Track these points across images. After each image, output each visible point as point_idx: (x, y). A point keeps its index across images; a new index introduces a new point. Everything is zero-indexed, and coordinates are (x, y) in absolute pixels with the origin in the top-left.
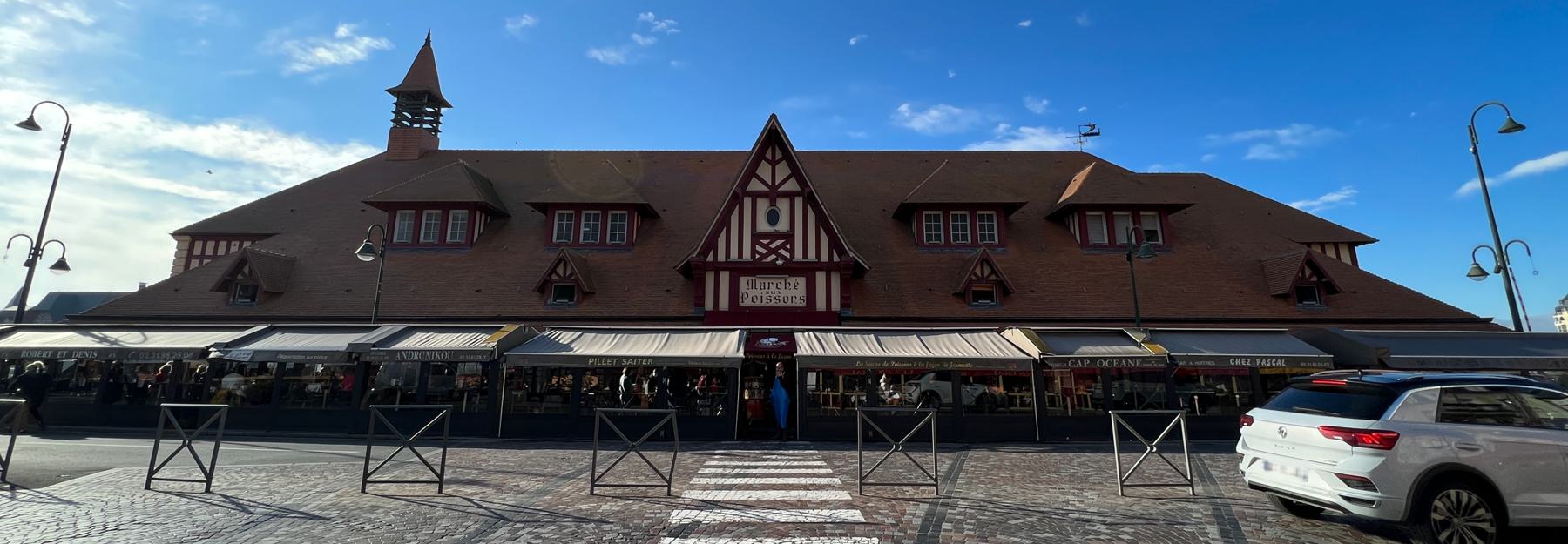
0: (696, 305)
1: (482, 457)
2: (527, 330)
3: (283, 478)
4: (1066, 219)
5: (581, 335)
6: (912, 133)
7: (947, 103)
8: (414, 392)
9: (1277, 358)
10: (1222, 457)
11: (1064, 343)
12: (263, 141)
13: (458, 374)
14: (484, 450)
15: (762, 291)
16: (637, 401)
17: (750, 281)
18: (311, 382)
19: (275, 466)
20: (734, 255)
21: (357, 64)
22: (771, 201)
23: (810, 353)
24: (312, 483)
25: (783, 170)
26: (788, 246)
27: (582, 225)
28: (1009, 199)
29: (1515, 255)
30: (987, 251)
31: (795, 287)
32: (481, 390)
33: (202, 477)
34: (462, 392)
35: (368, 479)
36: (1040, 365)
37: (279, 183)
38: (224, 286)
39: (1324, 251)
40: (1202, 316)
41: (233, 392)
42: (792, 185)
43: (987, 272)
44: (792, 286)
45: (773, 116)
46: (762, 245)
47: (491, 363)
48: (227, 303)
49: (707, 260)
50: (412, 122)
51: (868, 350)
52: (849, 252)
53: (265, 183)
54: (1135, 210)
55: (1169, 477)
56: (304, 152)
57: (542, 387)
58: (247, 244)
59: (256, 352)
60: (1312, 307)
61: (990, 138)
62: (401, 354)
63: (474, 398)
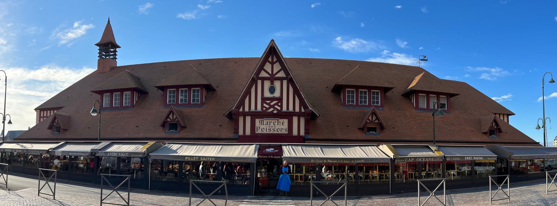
0: (235, 133)
1: (144, 197)
2: (158, 144)
3: (75, 198)
4: (410, 96)
5: (181, 146)
6: (342, 51)
7: (360, 38)
8: (115, 169)
9: (480, 157)
10: (458, 195)
11: (402, 151)
12: (55, 72)
13: (131, 163)
14: (144, 195)
15: (267, 126)
16: (208, 177)
17: (261, 121)
18: (80, 164)
19: (72, 193)
20: (253, 108)
21: (83, 36)
22: (271, 82)
23: (289, 156)
24: (84, 201)
25: (277, 67)
26: (280, 104)
27: (180, 95)
28: (387, 85)
29: (547, 121)
30: (375, 109)
31: (283, 124)
32: (141, 169)
33: (52, 194)
34: (133, 170)
35: (102, 202)
36: (393, 160)
37: (62, 87)
38: (50, 127)
39: (500, 117)
40: (458, 140)
41: (57, 166)
42: (282, 74)
43: (374, 119)
44: (281, 124)
45: (273, 41)
46: (267, 104)
47: (144, 158)
48: (52, 134)
49: (240, 111)
50: (106, 56)
51: (317, 155)
52: (309, 107)
53: (58, 88)
54: (438, 94)
55: (438, 204)
56: (68, 74)
57: (166, 169)
58: (55, 111)
59: (63, 152)
60: (494, 138)
61: (380, 56)
62: (109, 154)
63: (138, 173)
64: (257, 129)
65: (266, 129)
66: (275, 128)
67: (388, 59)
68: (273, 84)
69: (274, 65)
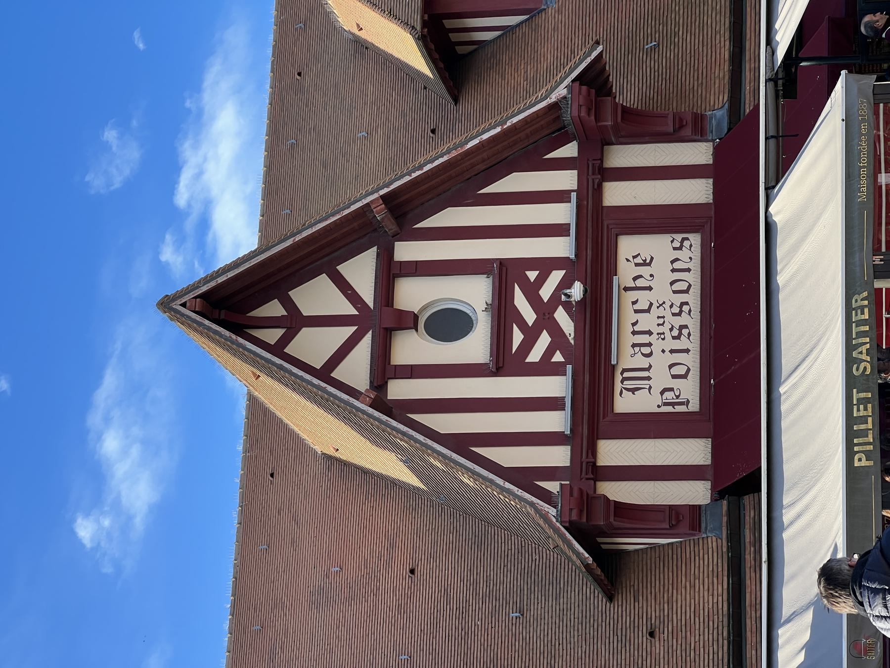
7: (85, 403)
17: (629, 384)
26: (532, 275)
31: (645, 264)
44: (645, 271)
45: (165, 304)
52: (553, 98)
64: (673, 404)
65: (672, 351)
66: (667, 306)
67: (215, 240)
68: (416, 317)
69: (307, 311)
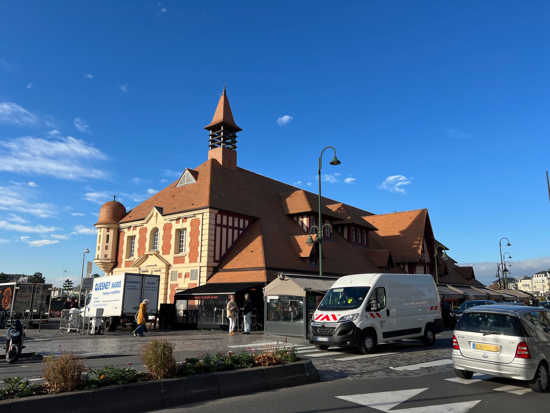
7: (19, 104)
